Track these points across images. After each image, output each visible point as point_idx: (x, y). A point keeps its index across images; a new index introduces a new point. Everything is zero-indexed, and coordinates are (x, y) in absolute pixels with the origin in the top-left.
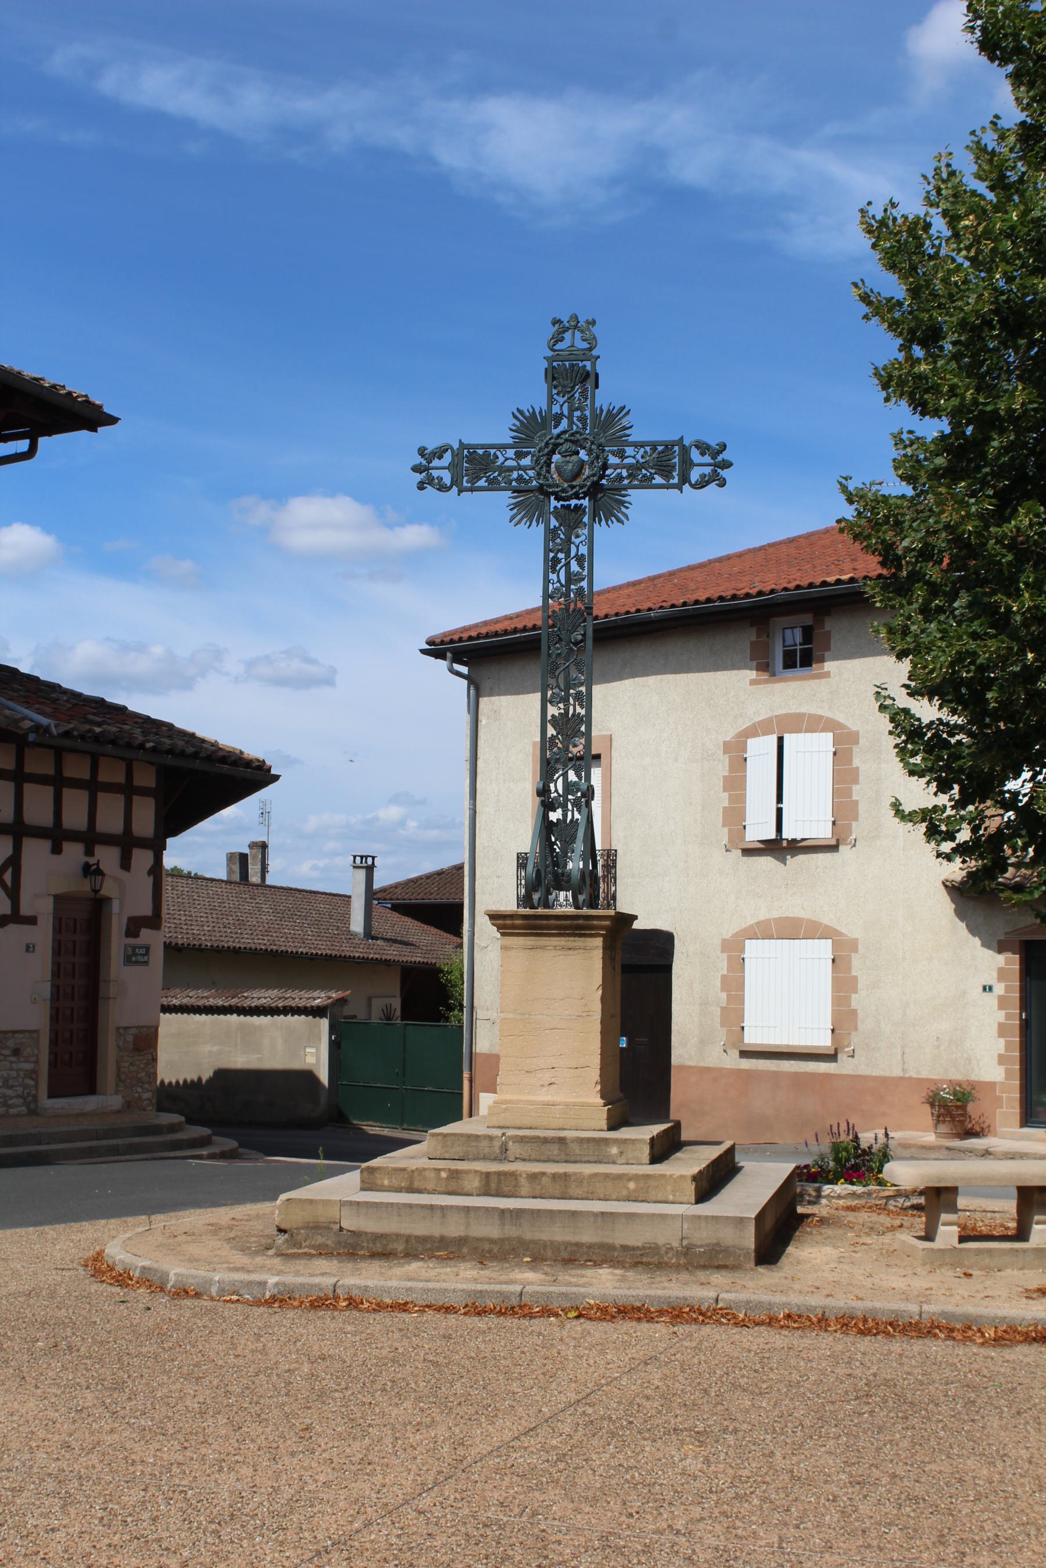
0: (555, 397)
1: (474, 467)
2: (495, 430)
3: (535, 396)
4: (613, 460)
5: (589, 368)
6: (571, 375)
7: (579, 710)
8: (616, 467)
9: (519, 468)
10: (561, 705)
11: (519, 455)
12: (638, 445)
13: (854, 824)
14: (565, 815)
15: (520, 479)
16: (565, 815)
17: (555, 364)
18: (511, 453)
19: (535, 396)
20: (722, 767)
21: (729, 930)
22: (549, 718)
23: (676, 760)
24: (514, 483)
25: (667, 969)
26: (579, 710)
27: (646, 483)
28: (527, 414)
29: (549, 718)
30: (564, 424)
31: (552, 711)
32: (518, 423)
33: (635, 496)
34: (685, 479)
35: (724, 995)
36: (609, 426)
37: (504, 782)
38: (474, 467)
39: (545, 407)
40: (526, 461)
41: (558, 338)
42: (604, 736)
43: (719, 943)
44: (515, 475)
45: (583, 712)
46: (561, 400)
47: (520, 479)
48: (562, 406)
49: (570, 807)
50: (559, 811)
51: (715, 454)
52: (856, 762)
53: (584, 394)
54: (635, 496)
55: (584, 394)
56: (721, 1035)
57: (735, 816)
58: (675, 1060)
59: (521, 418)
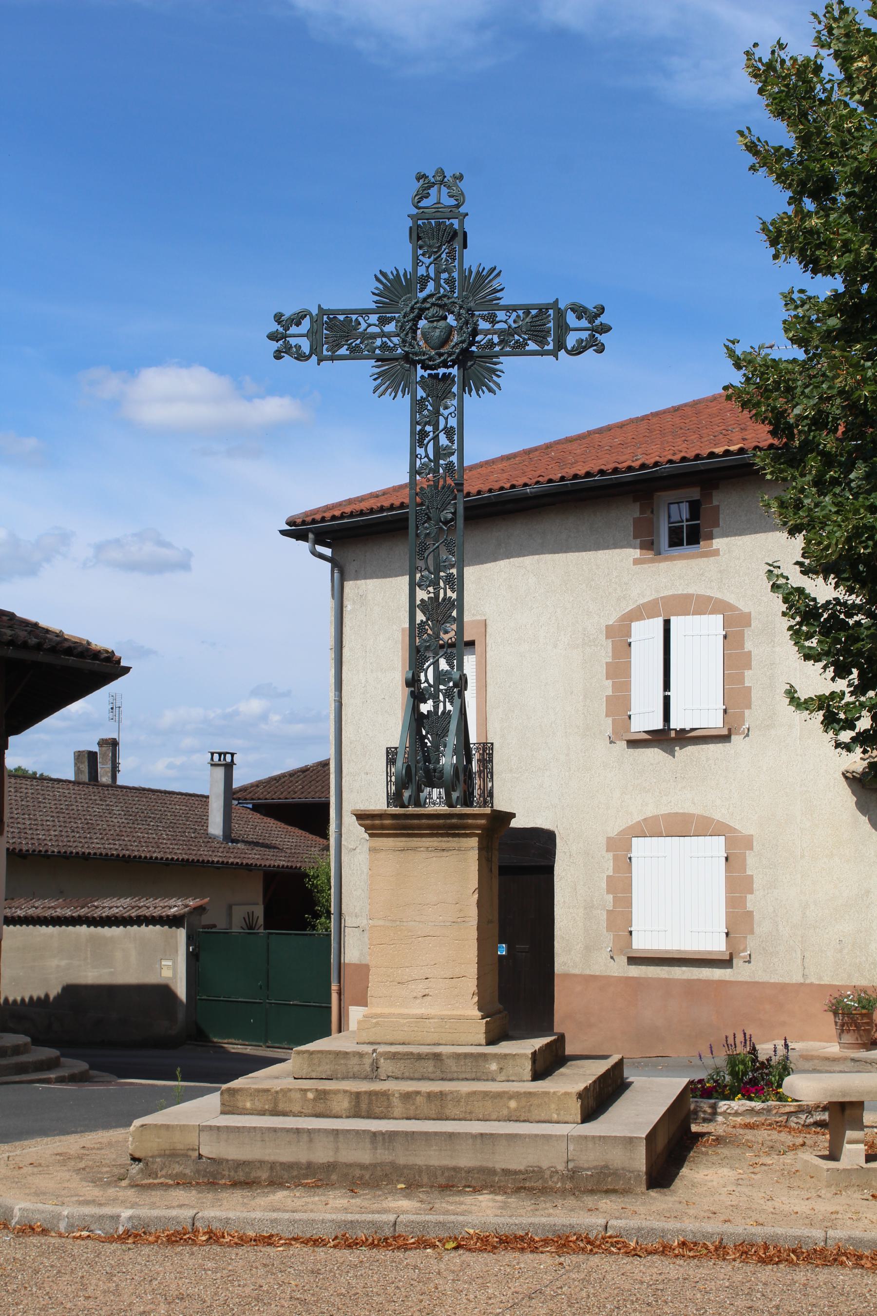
0: (421, 258)
1: (334, 334)
2: (356, 294)
3: (400, 257)
4: (483, 325)
5: (456, 226)
6: (439, 234)
7: (449, 593)
8: (486, 333)
9: (383, 335)
10: (431, 589)
11: (383, 321)
12: (416, 262)
13: (747, 712)
14: (436, 707)
15: (384, 346)
16: (436, 707)
17: (420, 222)
18: (373, 318)
19: (400, 257)
20: (605, 653)
21: (614, 828)
22: (418, 602)
23: (555, 646)
24: (377, 351)
25: (549, 870)
26: (449, 593)
27: (519, 350)
28: (391, 277)
29: (418, 602)
30: (431, 287)
31: (422, 595)
32: (381, 287)
33: (507, 364)
34: (560, 345)
35: (610, 897)
36: (480, 287)
37: (372, 671)
38: (334, 334)
39: (409, 269)
40: (391, 327)
41: (423, 194)
42: (479, 621)
43: (604, 841)
44: (378, 342)
45: (454, 596)
46: (427, 261)
47: (384, 346)
48: (428, 267)
49: (441, 698)
50: (430, 702)
51: (593, 318)
52: (748, 646)
53: (451, 255)
54: (507, 364)
55: (451, 255)
56: (608, 940)
57: (619, 705)
58: (558, 968)
59: (384, 281)
